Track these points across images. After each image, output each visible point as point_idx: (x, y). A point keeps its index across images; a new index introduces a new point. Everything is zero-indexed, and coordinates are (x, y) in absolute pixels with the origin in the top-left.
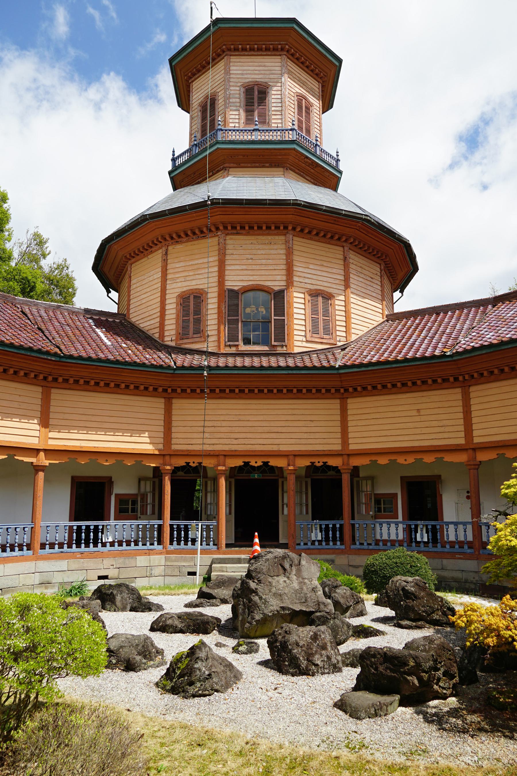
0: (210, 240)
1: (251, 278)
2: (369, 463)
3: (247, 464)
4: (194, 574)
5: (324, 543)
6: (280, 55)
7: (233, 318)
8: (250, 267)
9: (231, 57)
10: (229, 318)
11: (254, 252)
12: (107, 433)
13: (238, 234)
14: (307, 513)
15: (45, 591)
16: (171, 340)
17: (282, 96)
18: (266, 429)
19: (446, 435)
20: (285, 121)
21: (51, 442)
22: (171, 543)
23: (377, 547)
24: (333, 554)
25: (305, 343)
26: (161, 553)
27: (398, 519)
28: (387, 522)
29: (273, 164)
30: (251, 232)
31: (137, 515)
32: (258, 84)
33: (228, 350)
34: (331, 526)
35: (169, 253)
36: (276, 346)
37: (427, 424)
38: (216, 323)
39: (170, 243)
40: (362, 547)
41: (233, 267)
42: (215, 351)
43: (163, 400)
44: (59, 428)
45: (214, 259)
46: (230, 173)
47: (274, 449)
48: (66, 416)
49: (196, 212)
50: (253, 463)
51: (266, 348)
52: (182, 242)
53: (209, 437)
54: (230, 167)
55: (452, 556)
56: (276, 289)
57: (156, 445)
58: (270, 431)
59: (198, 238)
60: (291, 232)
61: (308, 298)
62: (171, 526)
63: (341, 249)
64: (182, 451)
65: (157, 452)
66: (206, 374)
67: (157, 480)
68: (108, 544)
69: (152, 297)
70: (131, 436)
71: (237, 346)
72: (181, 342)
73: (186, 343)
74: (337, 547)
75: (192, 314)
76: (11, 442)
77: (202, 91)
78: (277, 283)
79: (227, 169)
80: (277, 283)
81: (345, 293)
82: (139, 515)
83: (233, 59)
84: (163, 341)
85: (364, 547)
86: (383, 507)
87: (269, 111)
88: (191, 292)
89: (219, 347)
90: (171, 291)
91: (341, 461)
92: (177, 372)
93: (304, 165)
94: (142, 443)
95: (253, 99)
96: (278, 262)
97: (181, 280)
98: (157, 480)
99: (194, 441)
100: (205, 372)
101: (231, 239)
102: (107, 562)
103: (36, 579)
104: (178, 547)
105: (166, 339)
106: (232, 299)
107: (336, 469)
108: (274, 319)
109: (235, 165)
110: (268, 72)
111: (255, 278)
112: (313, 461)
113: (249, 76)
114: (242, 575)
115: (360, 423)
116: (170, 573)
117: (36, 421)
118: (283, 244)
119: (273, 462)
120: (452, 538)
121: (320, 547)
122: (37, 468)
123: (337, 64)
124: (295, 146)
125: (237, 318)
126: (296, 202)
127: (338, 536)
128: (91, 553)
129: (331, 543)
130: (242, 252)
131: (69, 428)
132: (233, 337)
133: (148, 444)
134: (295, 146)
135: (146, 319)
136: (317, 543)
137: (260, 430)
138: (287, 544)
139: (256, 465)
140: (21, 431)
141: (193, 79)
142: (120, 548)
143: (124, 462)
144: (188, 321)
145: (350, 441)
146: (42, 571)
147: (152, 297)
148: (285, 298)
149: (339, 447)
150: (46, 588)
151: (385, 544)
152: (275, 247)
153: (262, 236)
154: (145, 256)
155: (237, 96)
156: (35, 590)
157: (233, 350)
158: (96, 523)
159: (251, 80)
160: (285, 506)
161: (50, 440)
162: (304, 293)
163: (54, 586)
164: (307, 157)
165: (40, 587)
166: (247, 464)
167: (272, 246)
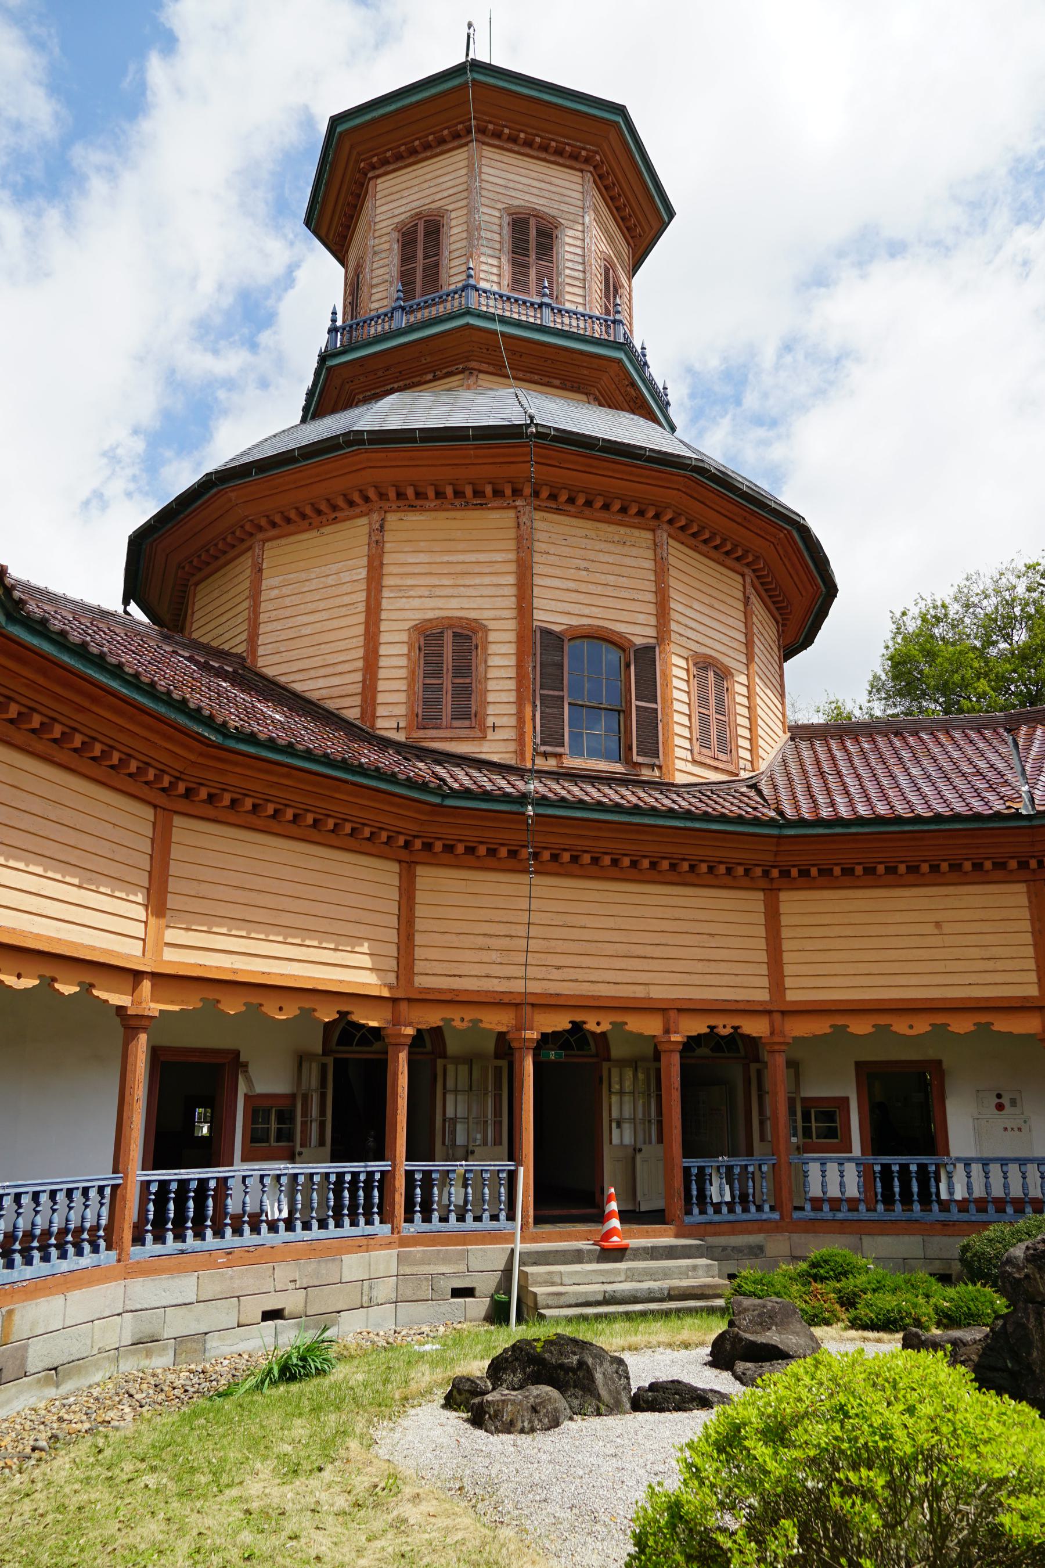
0: (494, 515)
1: (587, 611)
2: (828, 1030)
3: (577, 1027)
4: (467, 1292)
5: (739, 1209)
6: (581, 171)
7: (551, 693)
8: (583, 587)
9: (484, 147)
10: (543, 692)
11: (592, 555)
12: (289, 940)
13: (559, 511)
14: (322, 1143)
15: (145, 1363)
16: (398, 729)
17: (500, 262)
18: (622, 949)
19: (998, 978)
20: (590, 301)
21: (170, 955)
22: (409, 1220)
23: (982, 1217)
24: (760, 1231)
25: (689, 764)
26: (389, 1245)
27: (851, 1152)
28: (839, 1158)
29: (569, 384)
30: (587, 512)
31: (294, 1147)
32: (538, 216)
33: (541, 763)
34: (913, 1168)
35: (386, 528)
36: (640, 764)
37: (957, 953)
38: (513, 699)
39: (394, 507)
40: (819, 1215)
41: (548, 582)
42: (510, 760)
43: (395, 867)
44: (191, 919)
45: (504, 556)
46: (480, 382)
47: (638, 995)
48: (204, 889)
49: (478, 447)
50: (591, 1026)
51: (619, 768)
52: (423, 509)
53: (499, 960)
54: (480, 371)
55: (812, 1227)
56: (639, 641)
57: (382, 974)
58: (629, 954)
59: (466, 506)
60: (665, 526)
61: (693, 670)
62: (410, 1174)
63: (739, 578)
64: (440, 991)
65: (386, 993)
66: (532, 813)
67: (504, 1063)
68: (282, 1225)
69: (343, 622)
70: (336, 950)
71: (561, 755)
72: (421, 734)
73: (433, 739)
74: (765, 1217)
75: (450, 674)
76: (93, 948)
77: (404, 201)
78: (638, 630)
79: (476, 373)
80: (638, 630)
81: (748, 669)
82: (298, 1149)
83: (488, 152)
84: (373, 727)
85: (823, 1214)
86: (822, 1125)
87: (559, 275)
88: (446, 622)
89: (521, 753)
90: (394, 615)
91: (768, 1026)
92: (449, 802)
93: (621, 398)
94: (351, 968)
95: (527, 242)
96: (638, 584)
97: (420, 593)
98: (504, 1063)
99: (465, 969)
100: (530, 808)
101: (545, 520)
102: (284, 1272)
103: (125, 1330)
104: (426, 1226)
105: (380, 723)
106: (549, 654)
107: (753, 1042)
108: (637, 706)
109: (491, 369)
110: (556, 197)
111: (596, 612)
112: (713, 1023)
113: (518, 195)
114: (605, 1292)
115: (809, 945)
116: (409, 1294)
117: (140, 898)
118: (648, 548)
119: (593, 1024)
120: (815, 1191)
121: (731, 1217)
122: (133, 1023)
123: (666, 220)
124: (621, 355)
125: (561, 693)
126: (701, 464)
127: (915, 1189)
128: (248, 1250)
129: (898, 1207)
130: (566, 551)
131: (209, 919)
132: (552, 736)
133: (368, 972)
134: (621, 355)
135: (313, 673)
136: (725, 1209)
137: (610, 949)
138: (663, 1210)
139: (599, 1030)
140: (97, 919)
141: (378, 172)
142: (307, 1235)
143: (317, 1014)
144: (440, 687)
145: (788, 982)
146: (139, 1307)
147: (343, 622)
148: (657, 663)
149: (763, 996)
150: (149, 1354)
151: (1001, 1210)
152: (634, 552)
153: (606, 525)
154: (311, 527)
155: (496, 228)
156: (121, 1362)
157: (551, 764)
158: (183, 1174)
159: (522, 203)
160: (614, 1125)
161: (166, 949)
162: (687, 659)
163: (165, 1348)
164: (633, 384)
165: (134, 1353)
166: (577, 1027)
167: (626, 548)
